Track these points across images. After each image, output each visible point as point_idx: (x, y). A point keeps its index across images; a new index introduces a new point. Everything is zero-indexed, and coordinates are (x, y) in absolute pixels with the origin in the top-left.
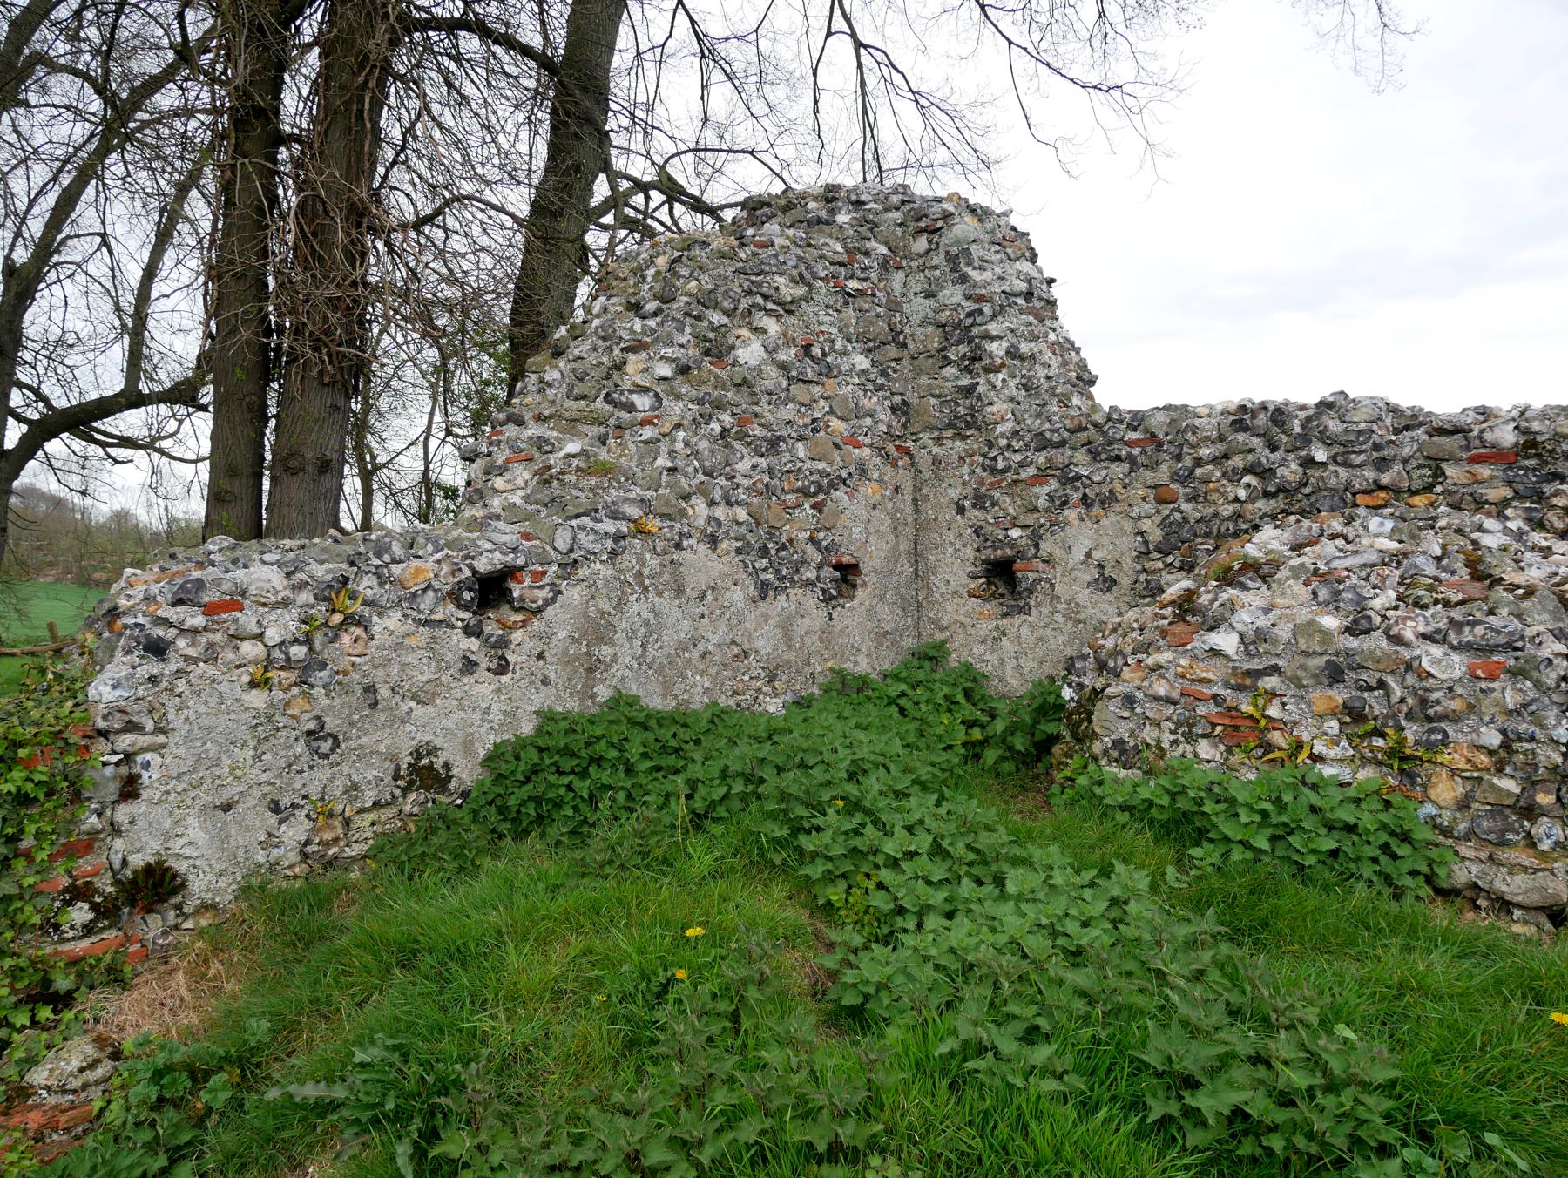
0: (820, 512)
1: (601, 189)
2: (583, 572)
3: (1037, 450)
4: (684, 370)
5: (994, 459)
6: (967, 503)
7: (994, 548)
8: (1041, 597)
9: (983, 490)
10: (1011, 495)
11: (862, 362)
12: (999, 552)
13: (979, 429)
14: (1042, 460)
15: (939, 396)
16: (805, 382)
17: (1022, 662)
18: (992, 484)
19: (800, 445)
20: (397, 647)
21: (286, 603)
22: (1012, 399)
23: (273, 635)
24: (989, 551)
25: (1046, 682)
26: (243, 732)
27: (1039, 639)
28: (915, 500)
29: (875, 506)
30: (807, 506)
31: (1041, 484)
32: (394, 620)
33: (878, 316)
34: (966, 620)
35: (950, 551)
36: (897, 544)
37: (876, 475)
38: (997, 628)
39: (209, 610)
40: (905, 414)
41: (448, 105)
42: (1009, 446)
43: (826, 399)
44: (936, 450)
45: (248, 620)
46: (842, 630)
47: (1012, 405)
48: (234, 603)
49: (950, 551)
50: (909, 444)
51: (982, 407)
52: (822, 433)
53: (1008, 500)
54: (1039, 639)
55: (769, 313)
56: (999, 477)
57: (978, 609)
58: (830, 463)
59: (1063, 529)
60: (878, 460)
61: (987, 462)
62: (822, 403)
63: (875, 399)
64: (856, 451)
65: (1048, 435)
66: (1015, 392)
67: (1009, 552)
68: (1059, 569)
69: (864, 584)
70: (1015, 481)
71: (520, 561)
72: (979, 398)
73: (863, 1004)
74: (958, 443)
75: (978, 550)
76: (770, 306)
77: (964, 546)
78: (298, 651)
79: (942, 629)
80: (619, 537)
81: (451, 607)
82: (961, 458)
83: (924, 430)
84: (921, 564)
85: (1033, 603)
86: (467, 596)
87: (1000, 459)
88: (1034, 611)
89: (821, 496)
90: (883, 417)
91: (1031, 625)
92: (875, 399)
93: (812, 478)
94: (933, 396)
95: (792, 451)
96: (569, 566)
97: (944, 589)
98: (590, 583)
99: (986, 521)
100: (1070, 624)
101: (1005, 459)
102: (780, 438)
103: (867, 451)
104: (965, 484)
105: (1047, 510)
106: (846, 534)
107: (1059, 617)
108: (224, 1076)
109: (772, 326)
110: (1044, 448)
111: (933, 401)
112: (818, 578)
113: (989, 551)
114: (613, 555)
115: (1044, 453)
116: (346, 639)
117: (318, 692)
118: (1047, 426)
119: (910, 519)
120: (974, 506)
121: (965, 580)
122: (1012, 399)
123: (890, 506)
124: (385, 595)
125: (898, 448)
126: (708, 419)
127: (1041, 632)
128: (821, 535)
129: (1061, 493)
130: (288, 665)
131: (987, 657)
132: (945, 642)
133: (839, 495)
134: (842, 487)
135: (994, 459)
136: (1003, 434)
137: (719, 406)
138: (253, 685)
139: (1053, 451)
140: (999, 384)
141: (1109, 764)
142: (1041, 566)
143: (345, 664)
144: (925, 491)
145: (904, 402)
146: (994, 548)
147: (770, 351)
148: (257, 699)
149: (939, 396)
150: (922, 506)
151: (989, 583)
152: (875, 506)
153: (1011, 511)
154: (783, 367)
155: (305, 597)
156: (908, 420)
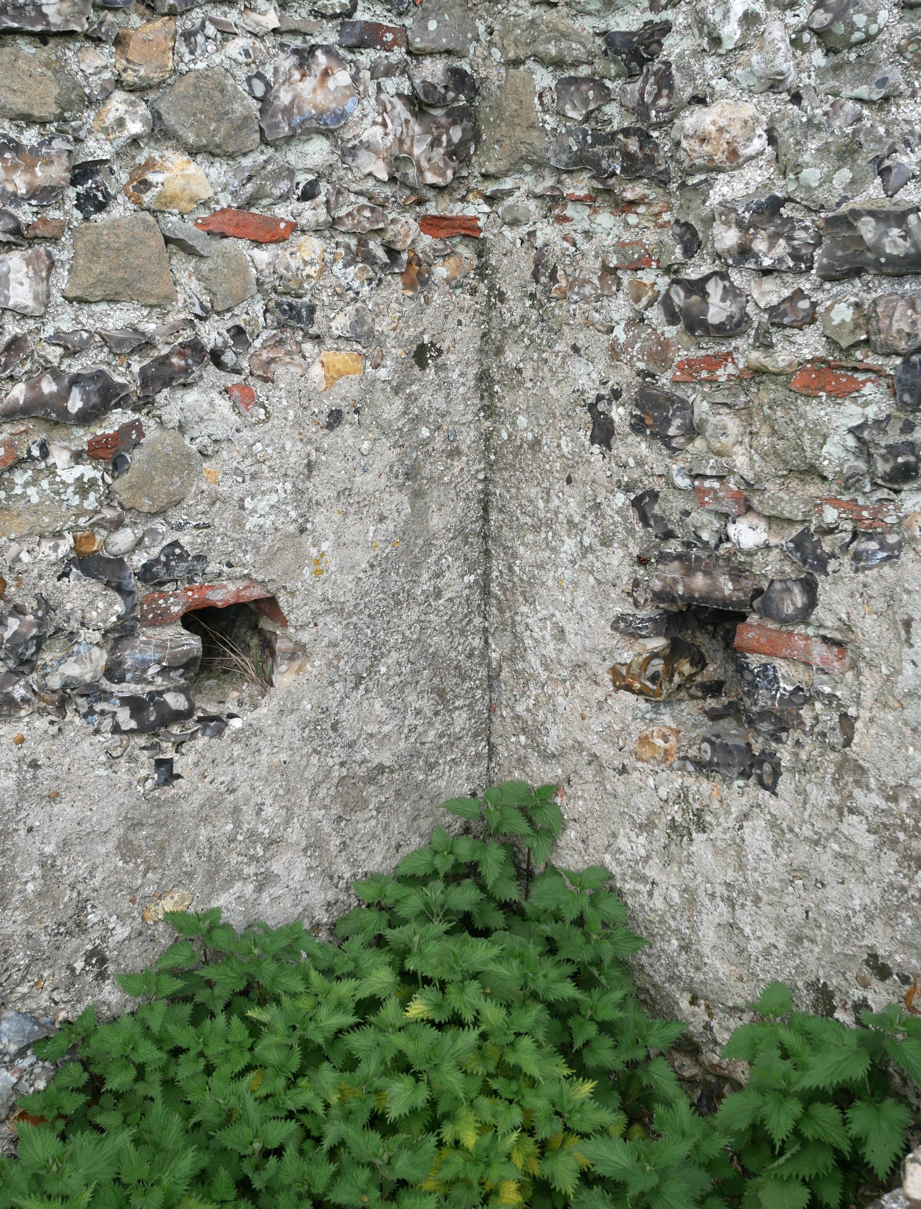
0: (118, 465)
3: (831, 276)
5: (698, 288)
6: (619, 414)
7: (689, 565)
8: (810, 749)
9: (665, 380)
10: (745, 412)
12: (699, 581)
13: (662, 181)
14: (843, 313)
15: (557, 64)
16: (43, 38)
17: (744, 918)
18: (690, 366)
22: (774, 84)
24: (673, 570)
25: (807, 998)
27: (797, 872)
28: (484, 377)
29: (335, 418)
30: (60, 457)
31: (838, 395)
34: (605, 750)
35: (569, 545)
36: (419, 515)
37: (341, 323)
38: (682, 796)
40: (456, 115)
42: (744, 252)
43: (139, 89)
44: (547, 232)
46: (212, 803)
47: (775, 104)
49: (569, 545)
50: (476, 209)
51: (674, 112)
52: (120, 209)
53: (733, 425)
54: (797, 872)
56: (713, 348)
57: (637, 728)
59: (892, 555)
60: (352, 275)
61: (679, 297)
62: (118, 104)
63: (342, 77)
64: (263, 256)
65: (868, 229)
66: (784, 63)
67: (727, 587)
68: (870, 681)
69: (299, 652)
70: (758, 373)
72: (665, 81)
73: (598, 1023)
74: (605, 219)
75: (642, 561)
77: (606, 542)
79: (547, 757)
82: (608, 271)
83: (515, 168)
84: (498, 566)
85: (785, 756)
87: (714, 289)
88: (785, 784)
89: (118, 418)
90: (373, 133)
91: (773, 824)
92: (342, 77)
93: (75, 366)
94: (541, 60)
97: (550, 650)
99: (667, 477)
100: (890, 860)
101: (731, 292)
103: (312, 247)
104: (615, 352)
105: (850, 482)
106: (222, 520)
107: (855, 826)
110: (856, 272)
111: (544, 78)
112: (113, 672)
113: (673, 570)
115: (854, 289)
118: (874, 190)
119: (468, 438)
120: (638, 427)
121: (607, 639)
122: (774, 84)
123: (392, 409)
125: (430, 224)
127: (802, 854)
128: (123, 539)
129: (894, 437)
131: (652, 871)
132: (552, 790)
134: (211, 373)
135: (698, 288)
136: (728, 208)
139: (882, 289)
140: (331, 257)
142: (819, 651)
144: (511, 356)
145: (459, 79)
146: (689, 565)
149: (557, 64)
150: (507, 400)
151: (672, 655)
152: (335, 418)
153: (740, 460)
156: (475, 136)
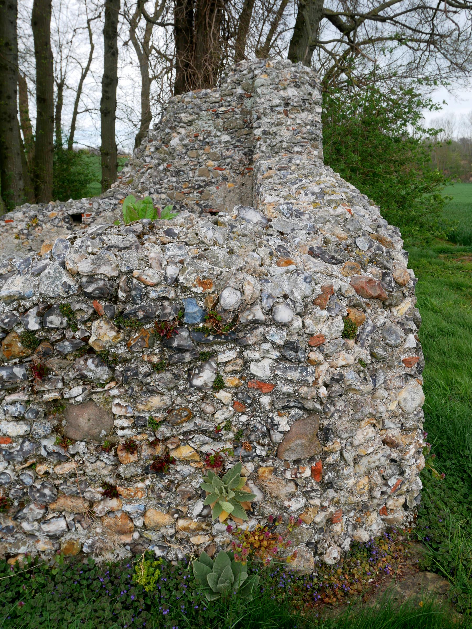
1: (150, 97)
2: (102, 214)
4: (157, 149)
11: (226, 138)
19: (191, 172)
20: (49, 232)
21: (22, 221)
23: (19, 228)
26: (13, 248)
29: (230, 191)
32: (49, 225)
33: (237, 118)
39: (6, 222)
41: (271, 93)
45: (14, 224)
48: (11, 220)
55: (181, 127)
58: (207, 177)
71: (82, 211)
76: (182, 124)
78: (25, 232)
80: (115, 205)
81: (63, 223)
86: (67, 220)
95: (188, 174)
96: (98, 213)
98: (105, 217)
102: (180, 171)
108: (343, 234)
109: (183, 131)
114: (113, 210)
116: (37, 229)
117: (30, 241)
124: (45, 219)
126: (159, 165)
128: (202, 202)
130: (23, 234)
133: (213, 188)
137: (164, 160)
138: (16, 238)
141: (375, 282)
143: (36, 235)
147: (181, 140)
148: (16, 241)
154: (185, 146)
155: (27, 219)
